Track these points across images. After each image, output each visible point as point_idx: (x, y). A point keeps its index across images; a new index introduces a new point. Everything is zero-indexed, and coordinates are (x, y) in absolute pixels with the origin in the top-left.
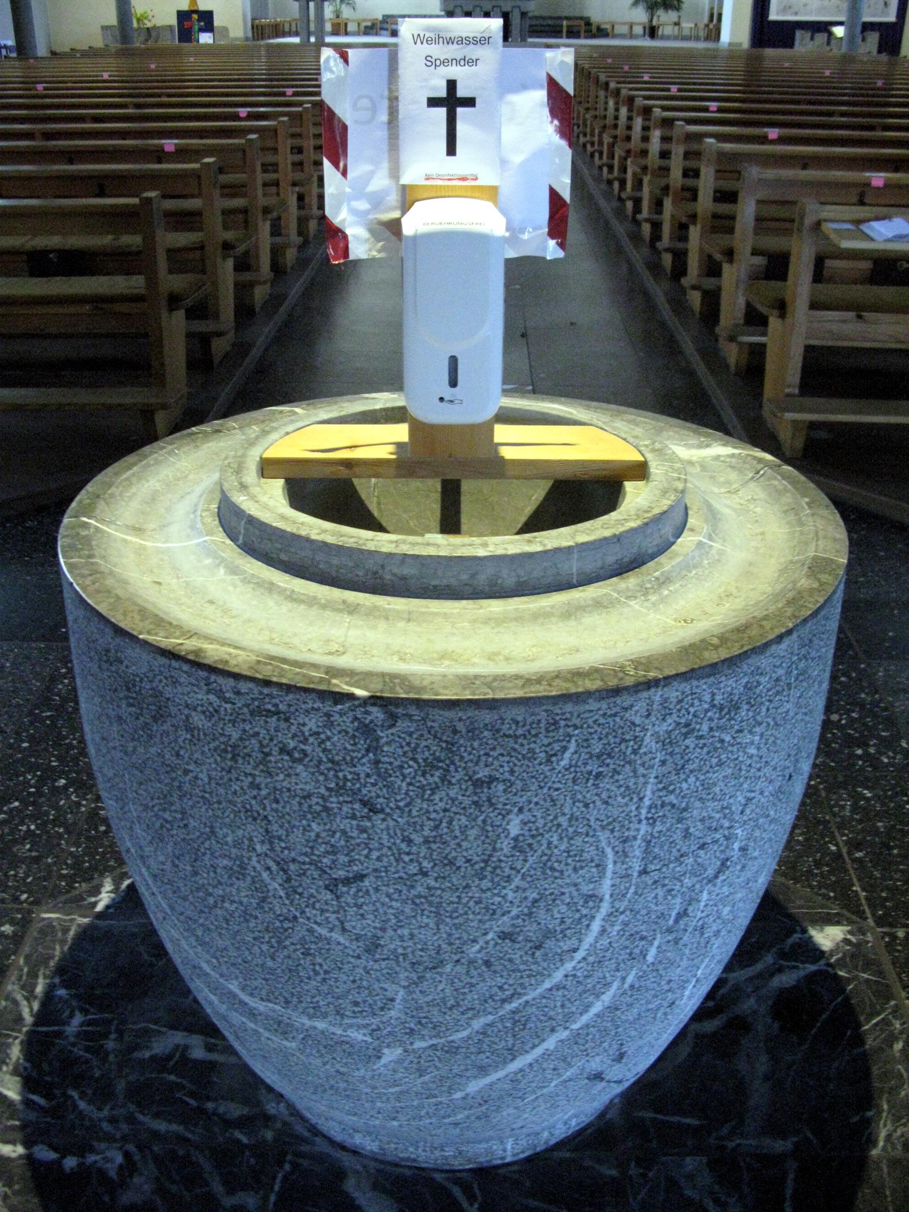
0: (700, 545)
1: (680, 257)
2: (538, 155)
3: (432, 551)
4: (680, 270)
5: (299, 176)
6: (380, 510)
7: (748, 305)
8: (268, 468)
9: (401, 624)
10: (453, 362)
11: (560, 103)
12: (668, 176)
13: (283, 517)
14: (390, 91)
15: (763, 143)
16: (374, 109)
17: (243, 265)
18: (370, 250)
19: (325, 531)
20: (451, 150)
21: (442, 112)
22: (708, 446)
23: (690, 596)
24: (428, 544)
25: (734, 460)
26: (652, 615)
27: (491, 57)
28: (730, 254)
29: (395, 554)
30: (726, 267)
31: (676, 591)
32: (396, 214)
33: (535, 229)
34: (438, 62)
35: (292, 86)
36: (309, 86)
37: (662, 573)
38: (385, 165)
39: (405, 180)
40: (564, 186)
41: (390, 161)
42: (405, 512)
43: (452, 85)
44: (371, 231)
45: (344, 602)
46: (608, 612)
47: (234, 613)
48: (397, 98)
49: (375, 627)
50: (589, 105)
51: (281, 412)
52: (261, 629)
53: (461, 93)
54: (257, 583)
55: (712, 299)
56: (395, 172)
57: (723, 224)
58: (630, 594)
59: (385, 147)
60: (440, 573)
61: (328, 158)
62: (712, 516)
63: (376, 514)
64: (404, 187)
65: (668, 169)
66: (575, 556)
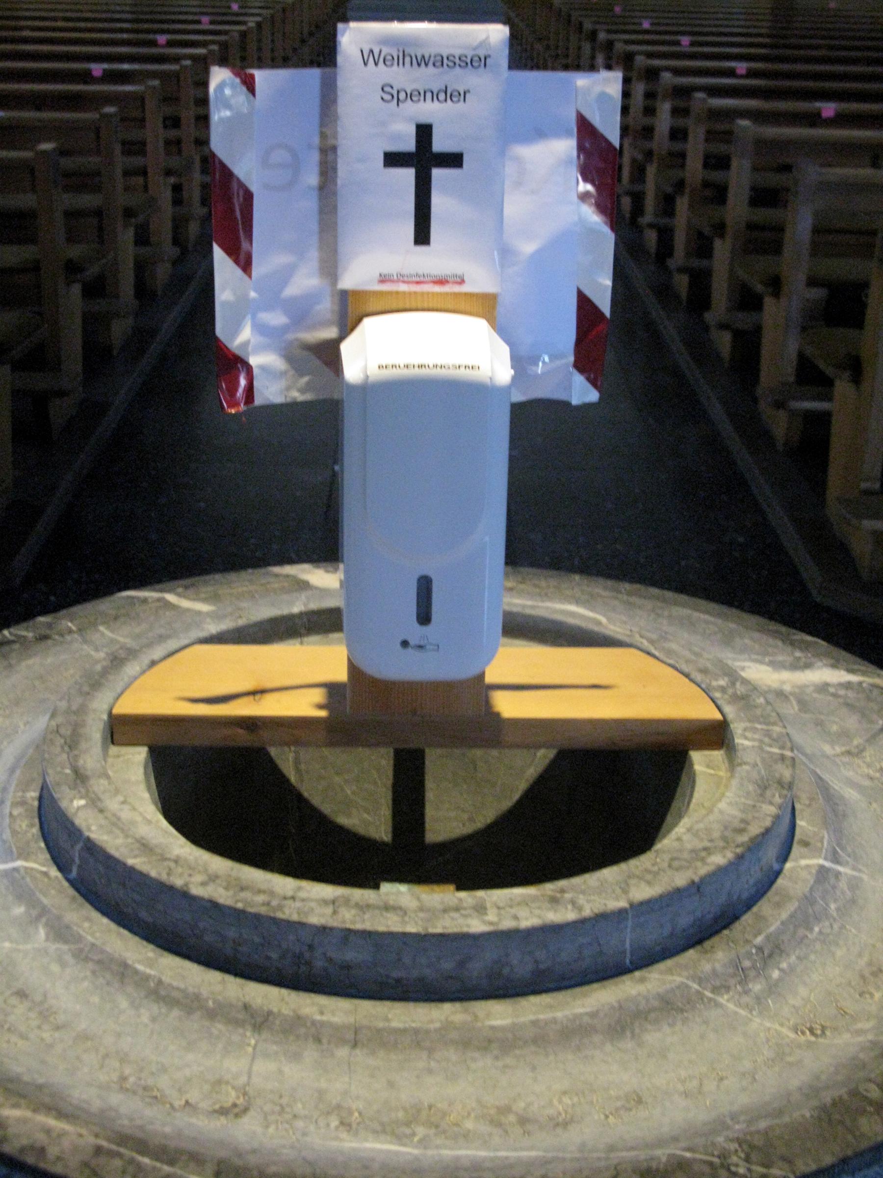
0: (822, 873)
1: (701, 281)
2: (558, 244)
3: (391, 923)
4: (700, 300)
5: (175, 162)
6: (298, 770)
7: (801, 356)
8: (121, 729)
9: (343, 1052)
10: (425, 587)
11: (597, 158)
12: (683, 166)
13: (145, 847)
14: (323, 136)
15: (813, 125)
16: (296, 166)
17: (95, 289)
18: (288, 389)
19: (213, 878)
20: (422, 236)
21: (407, 176)
22: (808, 666)
23: (815, 977)
24: (387, 908)
25: (851, 694)
26: (756, 1022)
27: (490, 88)
28: (775, 284)
29: (331, 929)
30: (768, 301)
31: (792, 969)
32: (331, 333)
33: (552, 358)
34: (402, 96)
35: (168, 32)
36: (189, 32)
37: (768, 938)
38: (314, 254)
39: (347, 282)
40: (602, 289)
41: (320, 249)
42: (337, 774)
43: (424, 132)
44: (289, 358)
45: (246, 1007)
46: (685, 1021)
47: (61, 1018)
48: (334, 149)
49: (296, 1057)
50: (569, 61)
51: (145, 601)
52: (106, 1056)
53: (439, 145)
54: (99, 962)
55: (748, 344)
56: (330, 267)
57: (765, 240)
58: (718, 983)
59: (314, 226)
60: (407, 960)
61: (221, 246)
62: (834, 812)
63: (293, 779)
64: (344, 295)
65: (683, 155)
66: (630, 923)
